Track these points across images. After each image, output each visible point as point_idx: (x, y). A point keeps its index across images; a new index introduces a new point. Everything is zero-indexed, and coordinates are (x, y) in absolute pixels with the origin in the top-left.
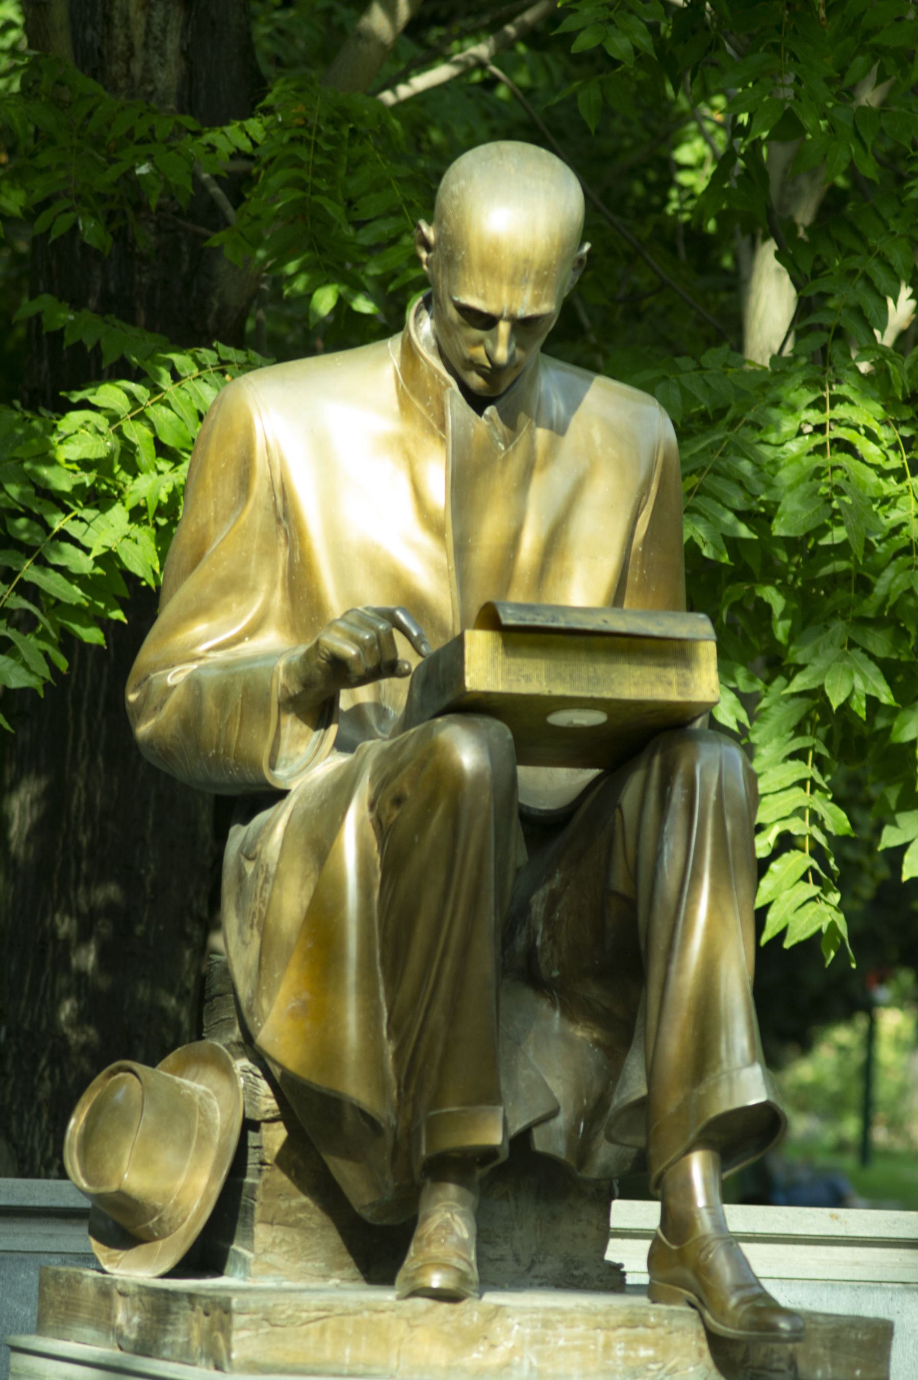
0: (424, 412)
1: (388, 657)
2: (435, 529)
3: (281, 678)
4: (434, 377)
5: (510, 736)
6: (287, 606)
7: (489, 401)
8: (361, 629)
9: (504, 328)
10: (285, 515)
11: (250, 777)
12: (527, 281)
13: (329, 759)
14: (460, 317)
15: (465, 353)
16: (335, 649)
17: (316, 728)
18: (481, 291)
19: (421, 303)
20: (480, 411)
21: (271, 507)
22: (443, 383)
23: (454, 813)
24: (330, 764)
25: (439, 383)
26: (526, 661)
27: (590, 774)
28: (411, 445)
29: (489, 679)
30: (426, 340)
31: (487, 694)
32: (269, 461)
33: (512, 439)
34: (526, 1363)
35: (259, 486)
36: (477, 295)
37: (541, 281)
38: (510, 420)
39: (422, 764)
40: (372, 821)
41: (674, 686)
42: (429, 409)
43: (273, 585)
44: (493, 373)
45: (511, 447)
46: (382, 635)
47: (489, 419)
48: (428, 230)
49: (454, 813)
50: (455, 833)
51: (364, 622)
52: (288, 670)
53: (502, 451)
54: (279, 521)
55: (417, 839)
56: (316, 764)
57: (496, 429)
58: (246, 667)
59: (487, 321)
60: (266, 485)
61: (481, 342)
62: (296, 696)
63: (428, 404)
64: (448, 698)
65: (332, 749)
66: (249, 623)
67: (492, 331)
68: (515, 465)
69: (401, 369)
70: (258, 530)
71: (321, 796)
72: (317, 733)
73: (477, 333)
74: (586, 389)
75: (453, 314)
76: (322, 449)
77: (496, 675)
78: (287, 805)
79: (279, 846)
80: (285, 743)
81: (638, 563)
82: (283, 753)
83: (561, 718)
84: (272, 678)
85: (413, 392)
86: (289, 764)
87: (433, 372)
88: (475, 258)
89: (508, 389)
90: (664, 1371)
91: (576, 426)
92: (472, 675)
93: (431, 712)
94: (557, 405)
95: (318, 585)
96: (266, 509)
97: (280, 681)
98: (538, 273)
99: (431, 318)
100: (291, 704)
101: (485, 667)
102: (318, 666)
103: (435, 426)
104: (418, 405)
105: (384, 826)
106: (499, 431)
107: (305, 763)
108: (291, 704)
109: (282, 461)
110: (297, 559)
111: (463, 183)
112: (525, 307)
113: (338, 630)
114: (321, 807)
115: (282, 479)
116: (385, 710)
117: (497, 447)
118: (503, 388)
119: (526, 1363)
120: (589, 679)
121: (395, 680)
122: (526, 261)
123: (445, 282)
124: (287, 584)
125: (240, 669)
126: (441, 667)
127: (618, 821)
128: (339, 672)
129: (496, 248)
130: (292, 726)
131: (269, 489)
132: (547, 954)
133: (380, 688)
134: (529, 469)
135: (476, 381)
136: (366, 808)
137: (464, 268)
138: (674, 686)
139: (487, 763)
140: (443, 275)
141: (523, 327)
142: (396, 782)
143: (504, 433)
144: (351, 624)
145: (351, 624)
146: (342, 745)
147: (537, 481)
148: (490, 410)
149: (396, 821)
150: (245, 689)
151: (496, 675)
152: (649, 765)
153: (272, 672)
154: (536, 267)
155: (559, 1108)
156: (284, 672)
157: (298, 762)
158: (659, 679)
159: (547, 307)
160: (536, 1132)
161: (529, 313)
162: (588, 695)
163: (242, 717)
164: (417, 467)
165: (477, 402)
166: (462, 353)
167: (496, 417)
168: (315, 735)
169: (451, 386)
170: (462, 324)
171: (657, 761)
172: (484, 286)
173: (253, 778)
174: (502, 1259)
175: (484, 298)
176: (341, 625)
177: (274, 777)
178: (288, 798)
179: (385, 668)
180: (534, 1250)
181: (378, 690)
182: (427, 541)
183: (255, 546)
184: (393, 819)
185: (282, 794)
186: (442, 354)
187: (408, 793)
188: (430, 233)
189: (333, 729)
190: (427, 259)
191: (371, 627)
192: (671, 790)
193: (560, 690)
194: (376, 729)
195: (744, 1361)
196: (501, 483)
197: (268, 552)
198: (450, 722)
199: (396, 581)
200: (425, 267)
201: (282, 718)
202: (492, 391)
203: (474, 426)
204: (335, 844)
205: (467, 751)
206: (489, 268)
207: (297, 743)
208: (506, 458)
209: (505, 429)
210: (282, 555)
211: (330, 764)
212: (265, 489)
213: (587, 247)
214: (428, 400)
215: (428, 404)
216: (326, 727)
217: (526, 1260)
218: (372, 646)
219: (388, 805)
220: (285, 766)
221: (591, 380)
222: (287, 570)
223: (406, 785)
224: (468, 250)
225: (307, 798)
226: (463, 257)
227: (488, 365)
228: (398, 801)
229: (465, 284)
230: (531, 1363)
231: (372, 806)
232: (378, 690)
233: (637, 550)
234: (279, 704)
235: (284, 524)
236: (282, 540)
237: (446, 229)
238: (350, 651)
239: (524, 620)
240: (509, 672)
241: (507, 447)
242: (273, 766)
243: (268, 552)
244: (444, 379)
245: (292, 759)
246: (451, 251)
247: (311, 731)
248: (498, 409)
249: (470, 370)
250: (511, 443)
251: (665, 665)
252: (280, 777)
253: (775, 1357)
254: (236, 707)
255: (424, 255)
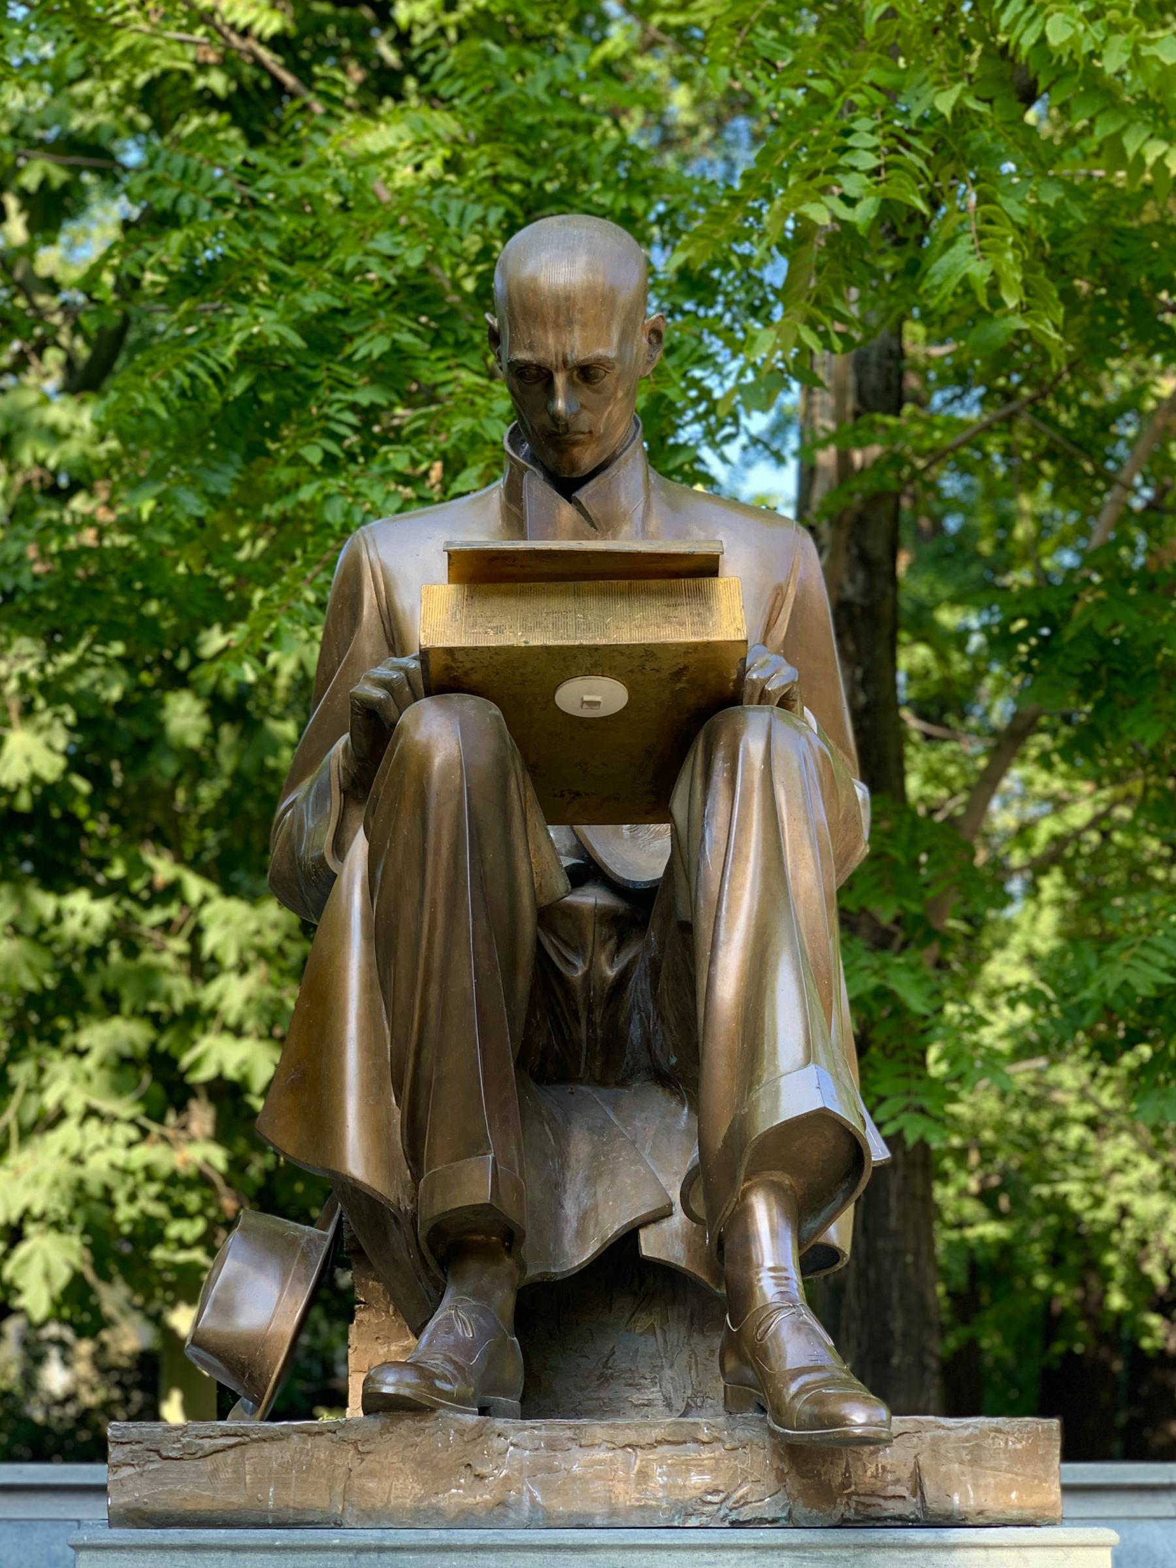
34: (526, 1498)
90: (730, 1503)
119: (526, 1498)
132: (660, 1037)
155: (671, 1205)
158: (667, 619)
160: (643, 1234)
174: (649, 1404)
180: (689, 1392)
195: (845, 1485)
217: (680, 1405)
230: (533, 1499)
234: (344, 791)
253: (889, 1477)
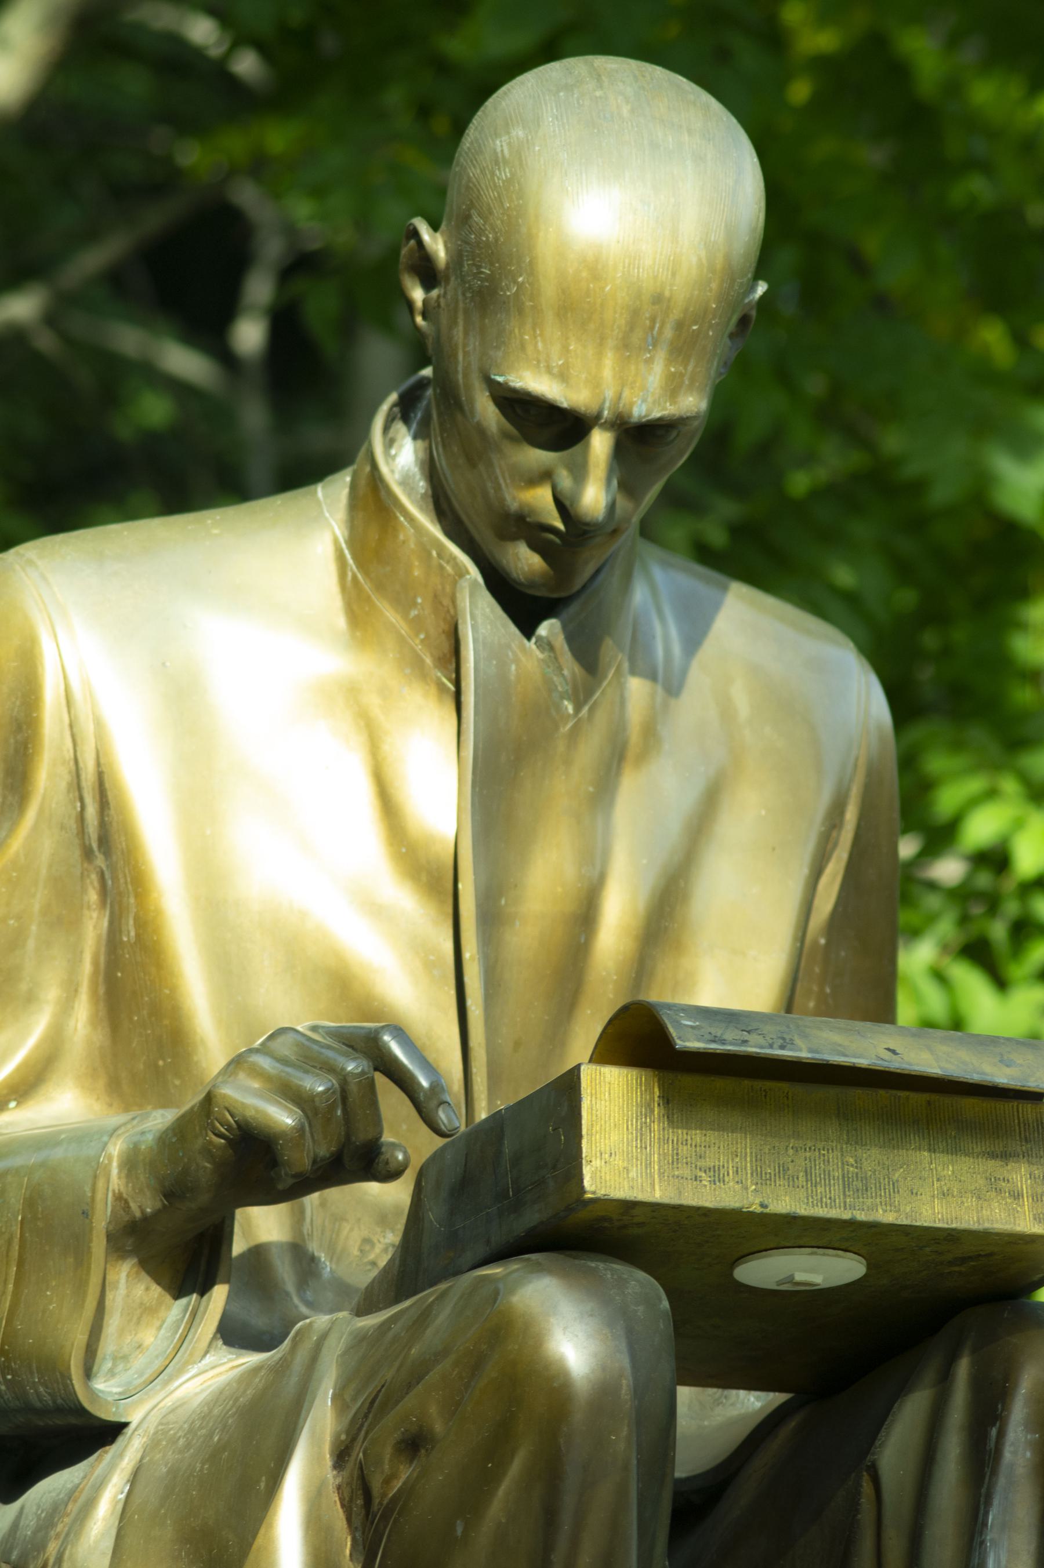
0: (404, 628)
1: (362, 1136)
2: (424, 878)
3: (116, 1180)
4: (430, 554)
5: (665, 1304)
6: (101, 1037)
7: (548, 608)
8: (306, 1072)
9: (600, 443)
10: (103, 843)
11: (39, 1392)
12: (655, 344)
13: (209, 1359)
14: (503, 420)
15: (508, 498)
16: (250, 1113)
17: (178, 1292)
18: (558, 362)
19: (394, 405)
20: (528, 629)
21: (73, 824)
22: (449, 569)
23: (549, 1472)
24: (212, 1374)
25: (442, 568)
26: (712, 1136)
27: (774, 1399)
28: (373, 701)
29: (633, 1174)
30: (405, 482)
31: (629, 1206)
32: (71, 726)
33: (589, 693)
35: (48, 777)
36: (549, 370)
37: (682, 347)
38: (586, 649)
39: (476, 1364)
40: (339, 1488)
41: (1026, 1202)
42: (417, 624)
43: (71, 990)
44: (571, 540)
45: (585, 710)
46: (353, 1088)
47: (547, 645)
48: (434, 240)
49: (549, 1472)
50: (550, 1515)
51: (309, 1057)
52: (130, 1163)
53: (569, 715)
54: (88, 854)
55: (459, 1530)
56: (180, 1371)
57: (560, 669)
58: (33, 1159)
59: (562, 428)
60: (65, 777)
61: (546, 476)
62: (145, 1219)
63: (414, 613)
64: (532, 1217)
65: (214, 1338)
66: (18, 1069)
67: (576, 449)
68: (589, 750)
69: (351, 542)
70: (44, 871)
71: (211, 1435)
72: (183, 1301)
73: (537, 457)
74: (717, 607)
75: (487, 412)
76: (184, 704)
77: (649, 1165)
78: (121, 1456)
79: (109, 1544)
80: (113, 1324)
81: (817, 970)
82: (108, 1345)
83: (764, 1271)
84: (95, 1177)
85: (380, 587)
86: (121, 1367)
87: (426, 546)
88: (549, 291)
89: (584, 587)
91: (700, 678)
92: (597, 1163)
93: (481, 1250)
94: (665, 635)
95: (174, 989)
96: (62, 827)
97: (112, 1184)
98: (679, 326)
99: (415, 438)
100: (134, 1238)
101: (624, 1147)
102: (207, 1150)
103: (428, 661)
104: (391, 614)
105: (376, 1501)
106: (566, 672)
107: (157, 1364)
108: (134, 1238)
109: (99, 724)
110: (129, 933)
111: (519, 133)
112: (647, 402)
113: (256, 1072)
114: (214, 1457)
115: (98, 764)
116: (313, 1259)
117: (558, 708)
118: (577, 585)
120: (846, 1183)
121: (373, 1188)
122: (658, 299)
123: (474, 343)
124: (102, 990)
125: (18, 1161)
126: (507, 1149)
127: (866, 1502)
128: (254, 1166)
129: (595, 269)
130: (129, 1286)
131: (70, 785)
133: (302, 1212)
134: (616, 758)
135: (525, 561)
136: (328, 1461)
137: (520, 311)
138: (1026, 1202)
139: (624, 1361)
140: (466, 334)
141: (639, 439)
142: (410, 1401)
143: (573, 674)
144: (284, 1061)
145: (284, 1061)
146: (233, 1334)
147: (630, 787)
148: (545, 628)
149: (408, 1492)
150: (31, 1203)
151: (649, 1165)
152: (946, 1377)
153: (97, 1171)
154: (676, 314)
156: (121, 1167)
157: (140, 1364)
158: (994, 1184)
159: (692, 403)
161: (656, 414)
162: (846, 1215)
163: (21, 1264)
164: (386, 748)
165: (524, 607)
166: (502, 500)
167: (560, 642)
168: (177, 1309)
169: (468, 572)
170: (506, 435)
171: (963, 1369)
172: (565, 350)
173: (47, 1398)
175: (563, 376)
176: (265, 1063)
177: (93, 1394)
178: (121, 1441)
179: (359, 1159)
181: (299, 1217)
182: (406, 902)
183: (37, 907)
184: (397, 1484)
185: (110, 1432)
186: (442, 505)
187: (438, 1427)
188: (437, 245)
189: (220, 1293)
190: (425, 302)
191: (329, 1068)
192: (1001, 1434)
193: (785, 1202)
194: (296, 1300)
196: (564, 785)
197: (63, 920)
198: (539, 1269)
199: (341, 981)
200: (419, 320)
201: (108, 1266)
202: (552, 585)
203: (517, 661)
204: (259, 1541)
205: (573, 1335)
206: (577, 310)
207: (138, 1322)
208: (574, 734)
209: (577, 669)
210: (93, 926)
211: (212, 1374)
212: (63, 785)
213: (761, 288)
214: (414, 604)
215: (414, 613)
216: (204, 1289)
218: (332, 1108)
219: (388, 1452)
220: (112, 1373)
221: (725, 589)
222: (102, 959)
223: (433, 1410)
224: (532, 270)
225: (173, 1441)
226: (520, 286)
227: (560, 525)
228: (414, 1444)
229: (523, 347)
231: (341, 1456)
232: (299, 1217)
233: (815, 942)
234: (110, 1237)
235: (100, 861)
236: (93, 896)
237: (481, 232)
238: (283, 1117)
239: (723, 1042)
240: (676, 1160)
241: (578, 708)
242: (88, 1373)
243: (63, 920)
244: (453, 559)
245: (125, 1358)
246: (490, 278)
247: (168, 1298)
248: (564, 627)
249: (514, 538)
250: (585, 702)
251: (1005, 1156)
252: (106, 1391)
254: (9, 1242)
255: (418, 295)
